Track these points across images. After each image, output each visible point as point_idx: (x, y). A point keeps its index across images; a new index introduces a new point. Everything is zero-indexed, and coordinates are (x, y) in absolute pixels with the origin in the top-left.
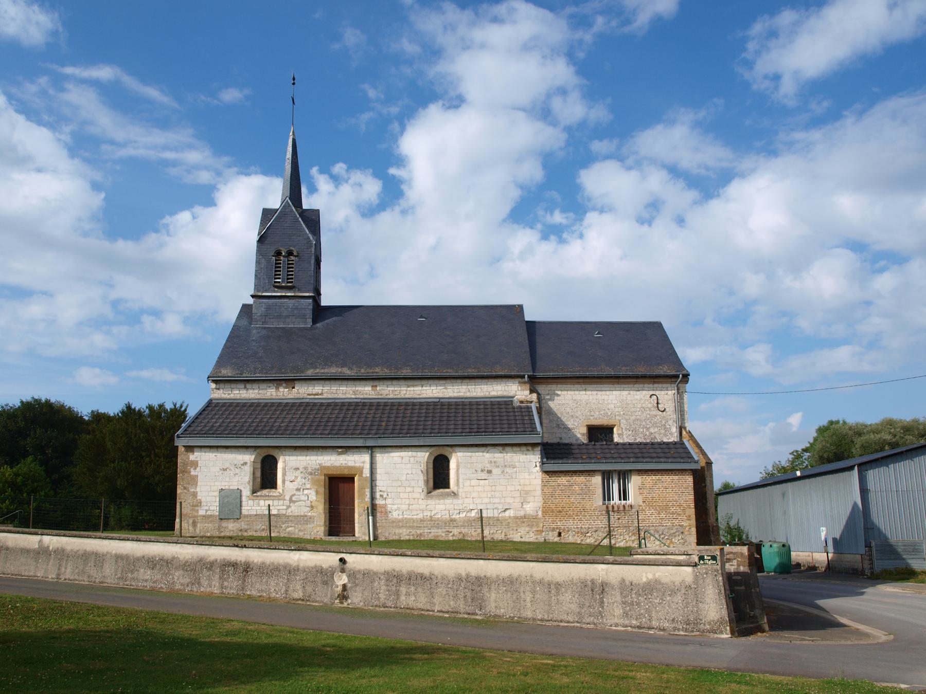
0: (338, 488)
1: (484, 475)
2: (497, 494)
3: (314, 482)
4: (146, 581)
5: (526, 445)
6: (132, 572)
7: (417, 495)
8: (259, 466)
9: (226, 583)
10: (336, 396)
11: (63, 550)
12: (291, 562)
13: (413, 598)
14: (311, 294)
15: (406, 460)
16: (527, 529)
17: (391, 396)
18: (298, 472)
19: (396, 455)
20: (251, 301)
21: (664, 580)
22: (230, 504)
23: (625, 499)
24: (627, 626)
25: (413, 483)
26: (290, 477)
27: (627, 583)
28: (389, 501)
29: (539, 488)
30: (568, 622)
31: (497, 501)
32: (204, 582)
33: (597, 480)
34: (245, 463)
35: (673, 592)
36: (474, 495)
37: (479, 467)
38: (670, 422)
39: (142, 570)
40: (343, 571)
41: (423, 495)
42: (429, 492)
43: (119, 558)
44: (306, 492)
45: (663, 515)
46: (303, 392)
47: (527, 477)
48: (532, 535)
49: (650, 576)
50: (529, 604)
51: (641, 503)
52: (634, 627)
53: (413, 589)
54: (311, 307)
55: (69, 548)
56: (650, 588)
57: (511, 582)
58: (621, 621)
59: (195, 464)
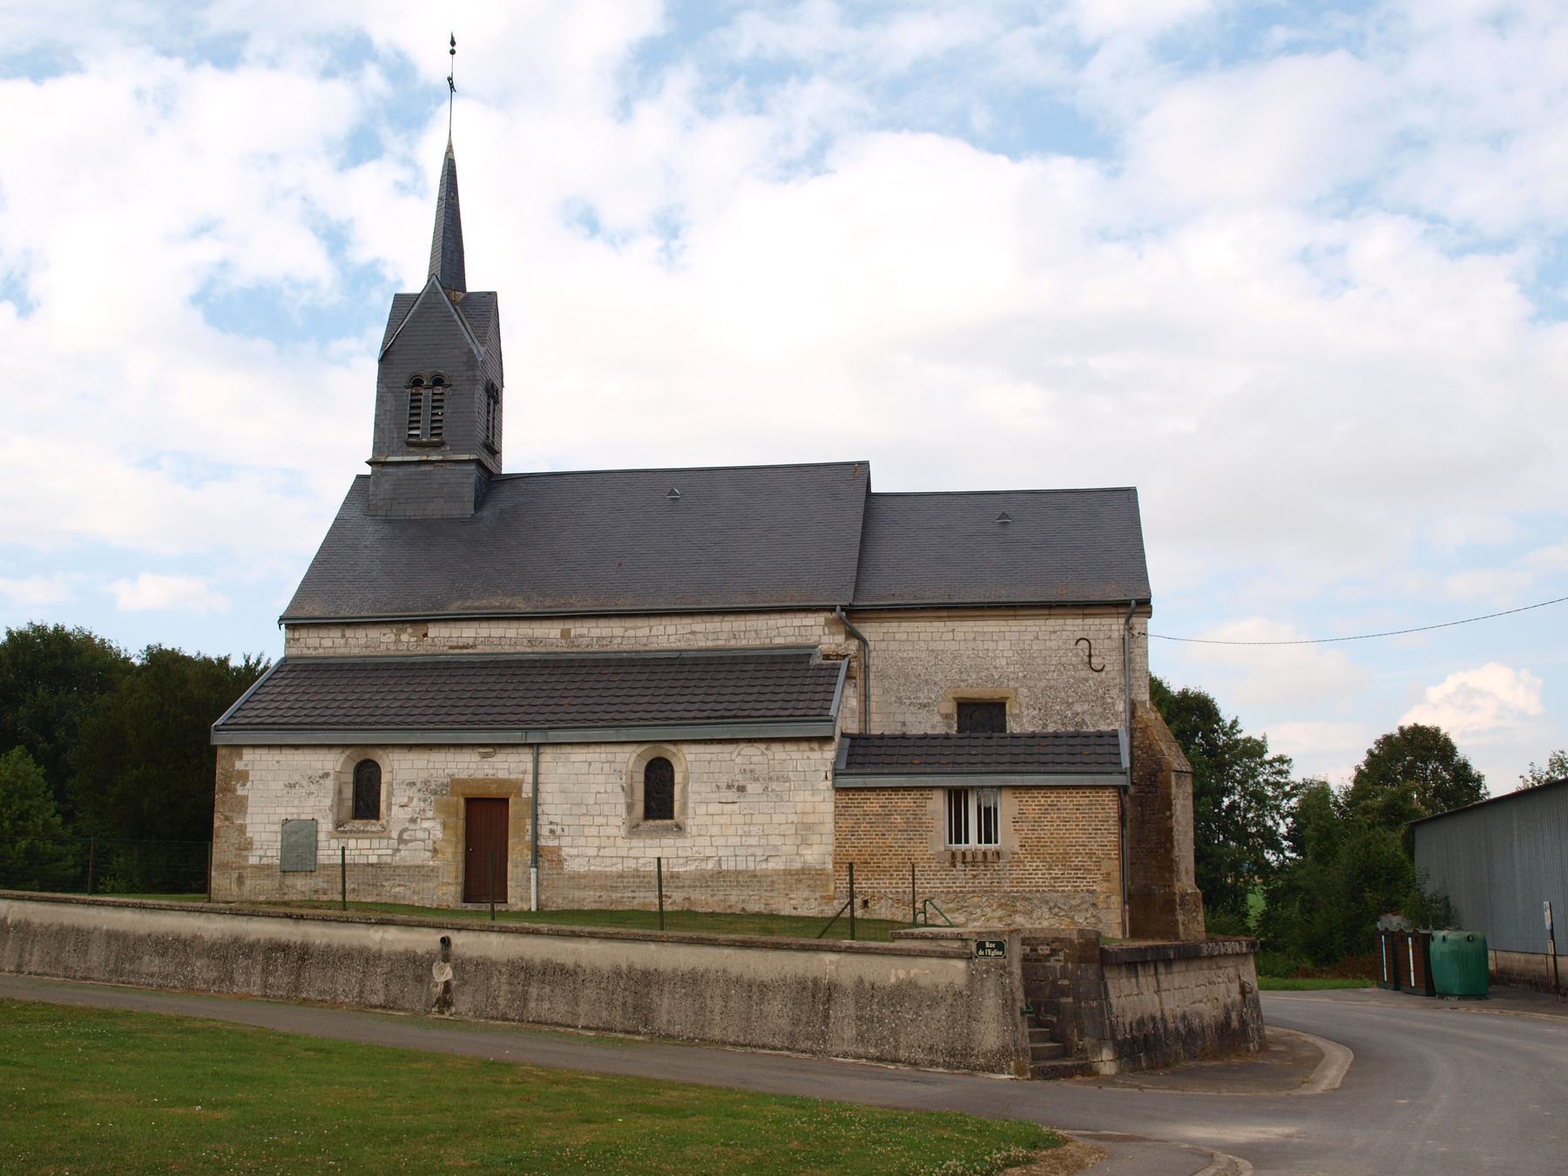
0: (485, 822)
1: (731, 795)
2: (754, 830)
3: (442, 808)
4: (152, 975)
5: (809, 740)
6: (132, 961)
7: (613, 831)
8: (350, 778)
9: (271, 980)
10: (498, 649)
11: (28, 924)
12: (370, 944)
13: (547, 1005)
14: (473, 457)
15: (596, 767)
16: (806, 894)
17: (596, 648)
18: (415, 789)
19: (579, 755)
20: (368, 470)
21: (922, 982)
22: (299, 843)
23: (988, 841)
24: (860, 1057)
25: (607, 809)
26: (400, 798)
27: (867, 985)
28: (565, 841)
29: (829, 819)
30: (774, 1048)
31: (753, 841)
32: (239, 978)
33: (938, 805)
34: (326, 775)
35: (935, 1002)
36: (715, 830)
37: (724, 780)
38: (1114, 692)
39: (146, 958)
40: (446, 959)
41: (623, 832)
42: (680, 828)
43: (112, 936)
44: (426, 824)
45: (1057, 872)
46: (444, 638)
47: (810, 799)
48: (814, 904)
49: (902, 974)
50: (718, 1018)
51: (1017, 849)
52: (871, 1059)
53: (547, 990)
54: (473, 480)
55: (36, 920)
56: (901, 994)
57: (693, 981)
58: (852, 1049)
59: (243, 777)
